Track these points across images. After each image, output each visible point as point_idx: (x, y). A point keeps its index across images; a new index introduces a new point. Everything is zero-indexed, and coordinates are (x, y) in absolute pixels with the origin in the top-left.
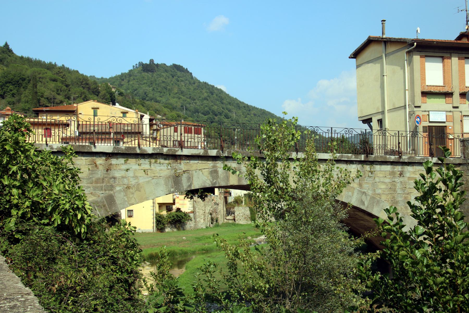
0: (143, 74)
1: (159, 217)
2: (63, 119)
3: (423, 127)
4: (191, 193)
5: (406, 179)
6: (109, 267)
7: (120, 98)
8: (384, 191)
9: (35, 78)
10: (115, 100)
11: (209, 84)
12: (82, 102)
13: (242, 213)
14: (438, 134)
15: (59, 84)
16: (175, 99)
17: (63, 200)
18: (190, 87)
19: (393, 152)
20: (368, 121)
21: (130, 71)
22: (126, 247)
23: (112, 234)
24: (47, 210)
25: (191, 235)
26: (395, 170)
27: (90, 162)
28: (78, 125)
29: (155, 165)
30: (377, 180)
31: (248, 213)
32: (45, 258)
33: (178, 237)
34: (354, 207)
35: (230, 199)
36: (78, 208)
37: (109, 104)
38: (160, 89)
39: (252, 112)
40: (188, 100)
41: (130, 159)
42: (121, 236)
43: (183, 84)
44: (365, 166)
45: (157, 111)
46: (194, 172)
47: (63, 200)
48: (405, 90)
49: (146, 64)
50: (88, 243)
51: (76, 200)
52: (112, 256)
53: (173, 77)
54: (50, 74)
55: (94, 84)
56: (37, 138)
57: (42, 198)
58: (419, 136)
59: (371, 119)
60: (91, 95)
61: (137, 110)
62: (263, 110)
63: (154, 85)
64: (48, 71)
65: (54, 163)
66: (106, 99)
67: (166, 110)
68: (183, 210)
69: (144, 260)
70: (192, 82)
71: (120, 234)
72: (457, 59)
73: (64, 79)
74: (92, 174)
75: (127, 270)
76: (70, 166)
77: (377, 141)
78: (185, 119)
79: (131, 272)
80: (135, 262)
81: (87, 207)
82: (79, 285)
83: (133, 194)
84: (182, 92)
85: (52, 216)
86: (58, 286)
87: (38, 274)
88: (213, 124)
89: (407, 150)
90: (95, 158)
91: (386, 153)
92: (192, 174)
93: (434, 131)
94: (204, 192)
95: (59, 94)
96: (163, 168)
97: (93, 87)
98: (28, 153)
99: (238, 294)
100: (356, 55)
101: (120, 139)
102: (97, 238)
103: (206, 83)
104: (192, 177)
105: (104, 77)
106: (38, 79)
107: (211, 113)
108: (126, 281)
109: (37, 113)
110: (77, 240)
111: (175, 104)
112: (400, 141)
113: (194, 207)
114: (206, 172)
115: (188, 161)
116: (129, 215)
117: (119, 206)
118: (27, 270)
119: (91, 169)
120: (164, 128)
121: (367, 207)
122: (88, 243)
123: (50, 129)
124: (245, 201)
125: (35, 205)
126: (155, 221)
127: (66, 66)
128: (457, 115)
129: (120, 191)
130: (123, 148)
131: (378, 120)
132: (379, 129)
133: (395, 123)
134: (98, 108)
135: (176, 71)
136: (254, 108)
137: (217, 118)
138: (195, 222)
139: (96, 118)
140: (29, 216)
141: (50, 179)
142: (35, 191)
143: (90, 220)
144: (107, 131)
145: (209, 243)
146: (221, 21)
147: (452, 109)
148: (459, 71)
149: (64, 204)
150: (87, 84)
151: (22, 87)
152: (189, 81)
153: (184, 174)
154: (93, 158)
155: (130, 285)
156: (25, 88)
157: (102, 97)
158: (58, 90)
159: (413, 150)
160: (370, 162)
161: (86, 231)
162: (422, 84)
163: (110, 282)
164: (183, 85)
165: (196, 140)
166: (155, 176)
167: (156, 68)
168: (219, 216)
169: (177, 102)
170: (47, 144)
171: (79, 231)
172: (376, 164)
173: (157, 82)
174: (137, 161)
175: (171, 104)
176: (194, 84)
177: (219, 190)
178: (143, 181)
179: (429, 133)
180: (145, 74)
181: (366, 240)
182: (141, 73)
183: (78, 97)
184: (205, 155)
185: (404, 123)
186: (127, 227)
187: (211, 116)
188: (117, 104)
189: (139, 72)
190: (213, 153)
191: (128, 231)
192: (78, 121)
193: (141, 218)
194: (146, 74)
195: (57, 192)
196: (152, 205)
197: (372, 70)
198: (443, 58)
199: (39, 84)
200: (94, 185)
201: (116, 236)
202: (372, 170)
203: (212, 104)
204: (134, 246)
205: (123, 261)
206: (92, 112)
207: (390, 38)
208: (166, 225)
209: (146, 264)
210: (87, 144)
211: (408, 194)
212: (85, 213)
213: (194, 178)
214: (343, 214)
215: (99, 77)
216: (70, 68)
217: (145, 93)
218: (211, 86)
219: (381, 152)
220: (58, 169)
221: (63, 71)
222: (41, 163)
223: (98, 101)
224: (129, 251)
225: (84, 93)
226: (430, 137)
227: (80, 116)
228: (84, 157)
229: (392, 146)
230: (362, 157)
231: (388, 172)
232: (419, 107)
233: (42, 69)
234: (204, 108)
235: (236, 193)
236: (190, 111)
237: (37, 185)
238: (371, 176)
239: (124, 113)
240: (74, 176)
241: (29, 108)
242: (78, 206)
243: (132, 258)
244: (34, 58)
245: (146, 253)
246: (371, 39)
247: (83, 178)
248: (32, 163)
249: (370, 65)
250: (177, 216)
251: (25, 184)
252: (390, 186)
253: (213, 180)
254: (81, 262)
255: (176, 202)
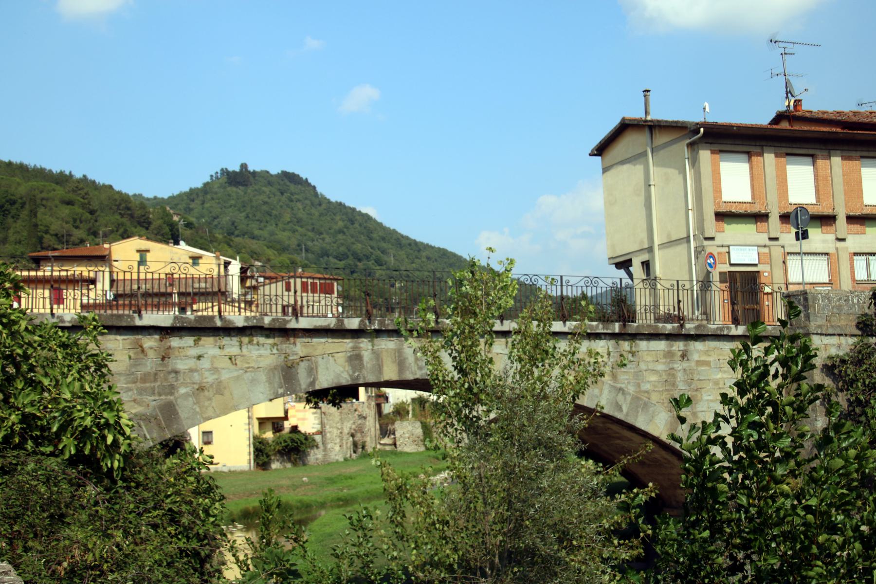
0: (229, 189)
1: (260, 443)
2: (83, 270)
3: (721, 273)
4: (316, 397)
5: (693, 364)
6: (165, 529)
7: (188, 232)
8: (654, 386)
9: (33, 200)
10: (178, 236)
11: (347, 205)
12: (118, 240)
13: (408, 433)
14: (745, 286)
15: (78, 209)
16: (287, 234)
17: (80, 411)
18: (313, 211)
19: (668, 318)
20: (624, 264)
21: (206, 185)
22: (196, 493)
23: (169, 470)
24: (50, 429)
25: (317, 473)
26: (674, 348)
27: (131, 344)
28: (112, 281)
29: (250, 347)
30: (643, 366)
31: (419, 431)
32: (45, 515)
33: (293, 478)
34: (605, 416)
35: (387, 409)
36: (107, 425)
37: (167, 243)
38: (259, 215)
39: (424, 254)
40: (310, 234)
41: (203, 338)
42: (185, 472)
43: (299, 205)
44: (621, 342)
45: (254, 255)
46: (320, 359)
47: (80, 411)
48: (687, 210)
49: (234, 172)
50: (125, 485)
51: (104, 410)
52: (170, 510)
53: (282, 194)
54: (60, 191)
55: (141, 208)
56: (36, 303)
57: (41, 407)
58: (714, 288)
59: (630, 261)
60: (136, 227)
61: (218, 253)
62: (444, 249)
63: (248, 210)
64: (58, 187)
65: (64, 346)
66: (162, 235)
67: (270, 252)
68: (302, 429)
69: (233, 521)
70: (316, 201)
71: (184, 470)
72: (773, 155)
73: (86, 201)
74: (135, 365)
75: (198, 533)
76: (92, 348)
77: (641, 299)
78: (304, 267)
79: (205, 537)
80: (212, 519)
81: (123, 421)
82: (107, 562)
83: (210, 399)
84: (299, 221)
85: (60, 441)
86: (69, 565)
87: (30, 543)
88: (355, 275)
89: (693, 313)
90: (140, 337)
91: (658, 319)
92: (316, 363)
93: (738, 280)
94: (342, 394)
95: (77, 227)
96: (263, 353)
97: (138, 213)
98: (16, 327)
99: (403, 574)
100: (601, 150)
101: (186, 303)
102: (142, 478)
103: (340, 205)
104: (317, 368)
105: (160, 196)
106: (39, 201)
107: (351, 257)
108: (196, 554)
109: (38, 262)
110: (106, 482)
111: (287, 242)
112: (681, 298)
113: (322, 424)
114: (341, 358)
115: (309, 340)
116: (206, 440)
117: (184, 423)
118: (10, 539)
119: (132, 356)
120: (264, 285)
121: (627, 415)
122: (125, 485)
123: (60, 290)
124: (413, 410)
125: (26, 419)
126: (252, 449)
127: (91, 177)
128: (777, 253)
129: (187, 395)
130: (192, 317)
131: (643, 263)
132: (645, 278)
133: (672, 267)
134: (148, 251)
135: (288, 183)
136: (427, 247)
137: (360, 265)
138: (325, 450)
139: (142, 268)
140: (17, 440)
141: (57, 372)
142: (28, 395)
143: (130, 445)
144: (163, 290)
145: (349, 487)
146: (364, 94)
147: (768, 243)
148: (777, 176)
149: (82, 418)
150: (129, 209)
151: (9, 216)
152: (311, 200)
153: (301, 363)
154: (137, 337)
155: (203, 562)
156: (16, 217)
157: (155, 232)
158: (75, 220)
159: (705, 313)
160: (630, 335)
161: (122, 465)
162: (715, 198)
163: (166, 555)
164: (301, 207)
165: (323, 303)
166: (249, 368)
167: (251, 179)
168: (368, 439)
169: (289, 238)
170: (52, 314)
171: (109, 465)
172: (641, 340)
173: (254, 204)
174: (216, 341)
175: (279, 242)
176: (320, 205)
177: (367, 391)
178: (227, 376)
179: (730, 283)
180: (232, 190)
181: (624, 472)
182: (225, 188)
183: (112, 232)
184: (339, 328)
185: (687, 267)
186: (197, 456)
187: (350, 261)
188: (182, 243)
189: (222, 186)
190: (353, 323)
191: (199, 464)
192: (111, 273)
193: (227, 443)
194: (234, 189)
195: (68, 396)
196: (247, 421)
197: (629, 176)
198: (749, 154)
199: (41, 210)
200: (139, 385)
201: (178, 473)
202: (634, 349)
203: (353, 240)
204: (210, 490)
205: (190, 517)
206: (137, 257)
207: (658, 121)
208: (273, 458)
209: (235, 527)
210: (127, 312)
211: (697, 390)
212: (120, 433)
213: (320, 370)
214: (581, 423)
215: (151, 196)
216: (97, 181)
217: (233, 224)
218: (350, 208)
219: (648, 318)
220: (72, 355)
221: (85, 186)
222: (39, 345)
223: (148, 239)
224: (201, 500)
225: (122, 224)
226: (733, 291)
227: (115, 264)
228: (120, 334)
229: (667, 308)
230: (617, 327)
231: (662, 353)
232: (712, 239)
233: (47, 184)
234: (338, 248)
235: (397, 396)
236: (313, 253)
237: (33, 384)
238: (632, 359)
239: (195, 259)
240: (100, 366)
241: (23, 253)
242: (107, 420)
243: (206, 511)
244: (32, 165)
245: (234, 505)
246: (627, 122)
247: (119, 374)
248: (23, 346)
249: (626, 167)
250: (293, 440)
251: (9, 383)
252: (665, 377)
253: (354, 372)
254: (112, 521)
255: (289, 415)
